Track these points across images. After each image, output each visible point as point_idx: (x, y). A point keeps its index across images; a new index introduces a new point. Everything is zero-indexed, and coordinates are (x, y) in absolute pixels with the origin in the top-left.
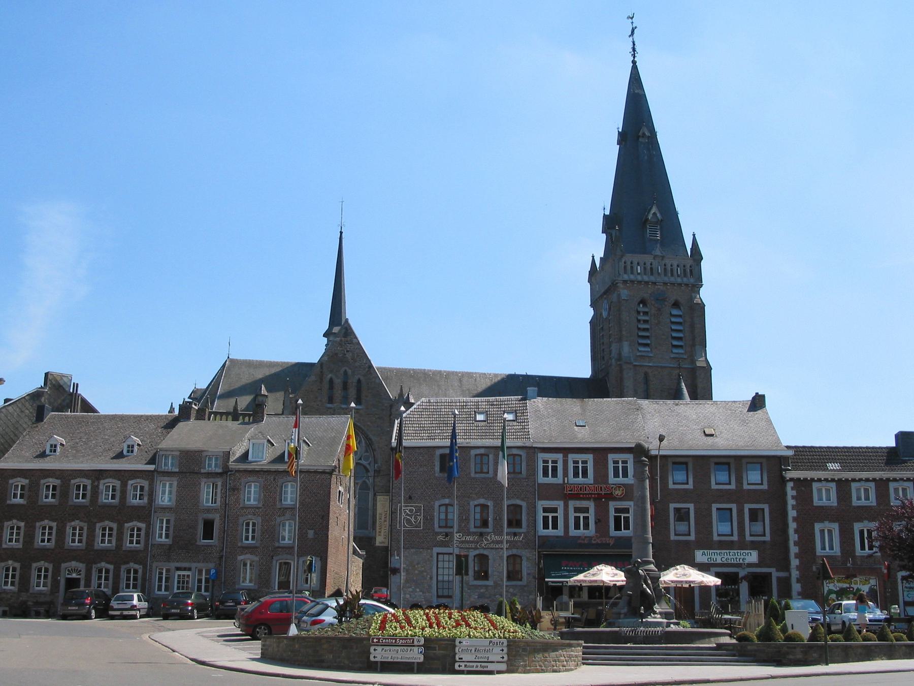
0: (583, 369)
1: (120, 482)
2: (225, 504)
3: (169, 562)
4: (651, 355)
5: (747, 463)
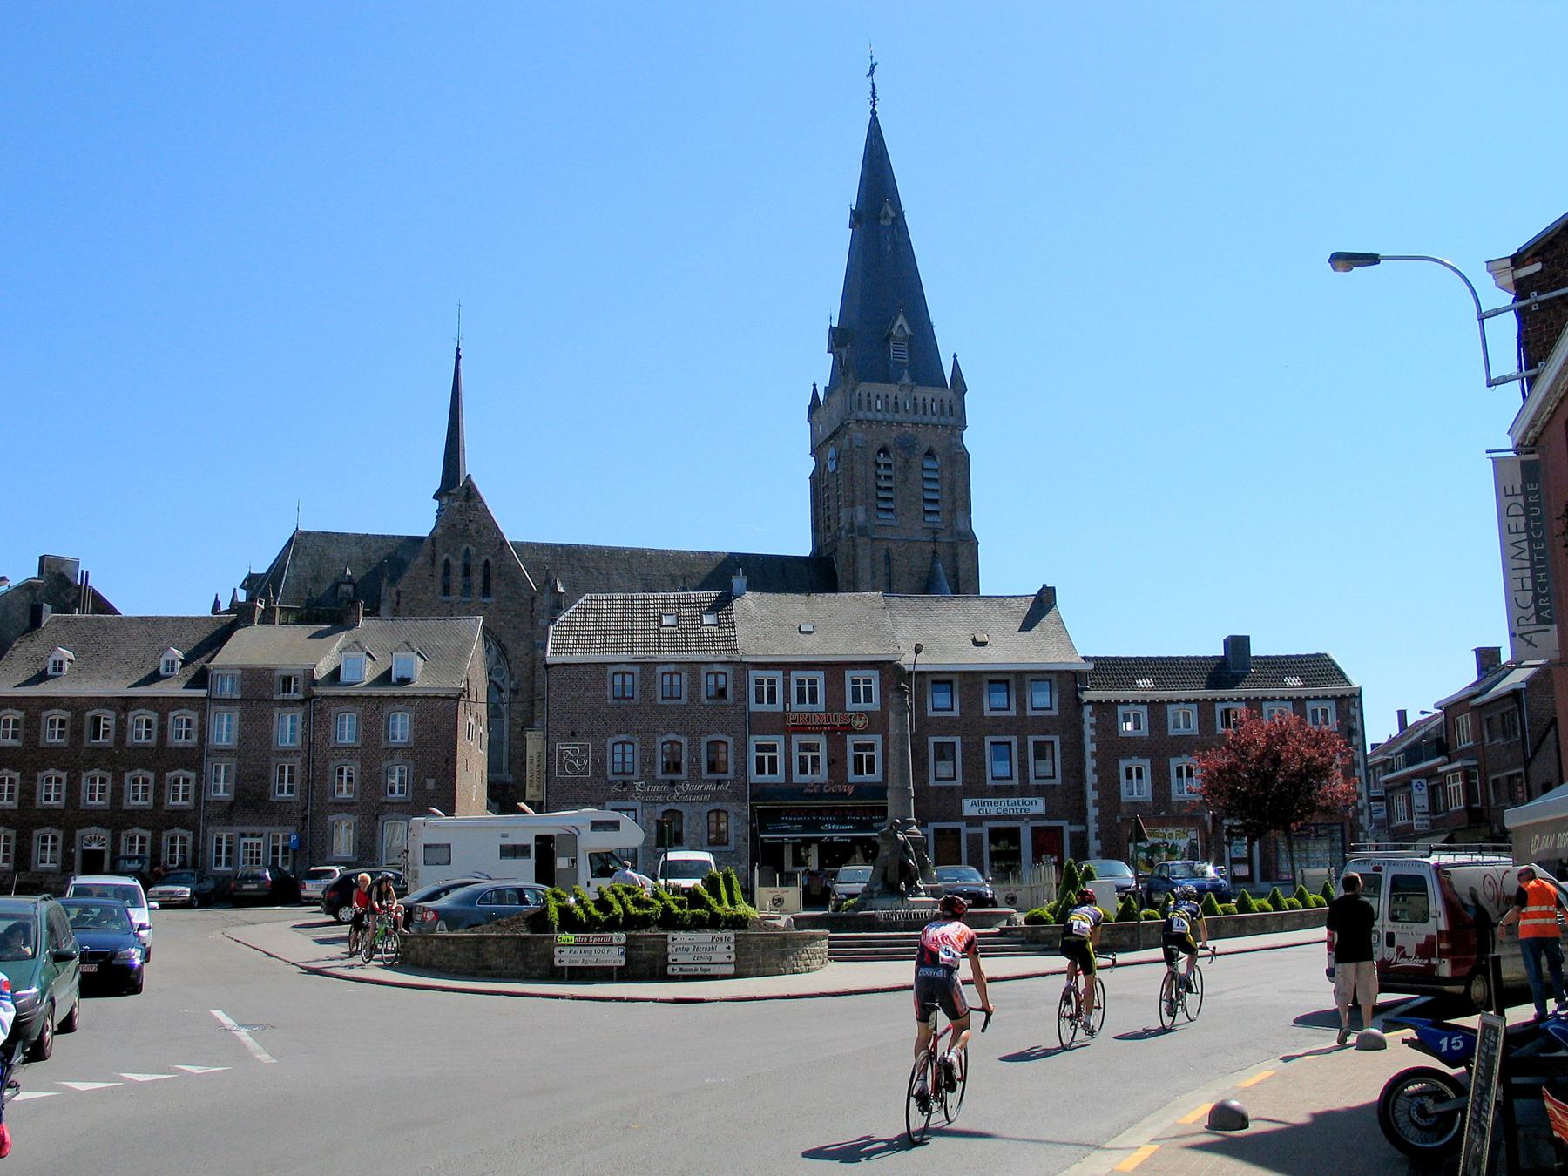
0: (799, 543)
1: (157, 714)
2: (310, 745)
4: (896, 524)
5: (1032, 680)
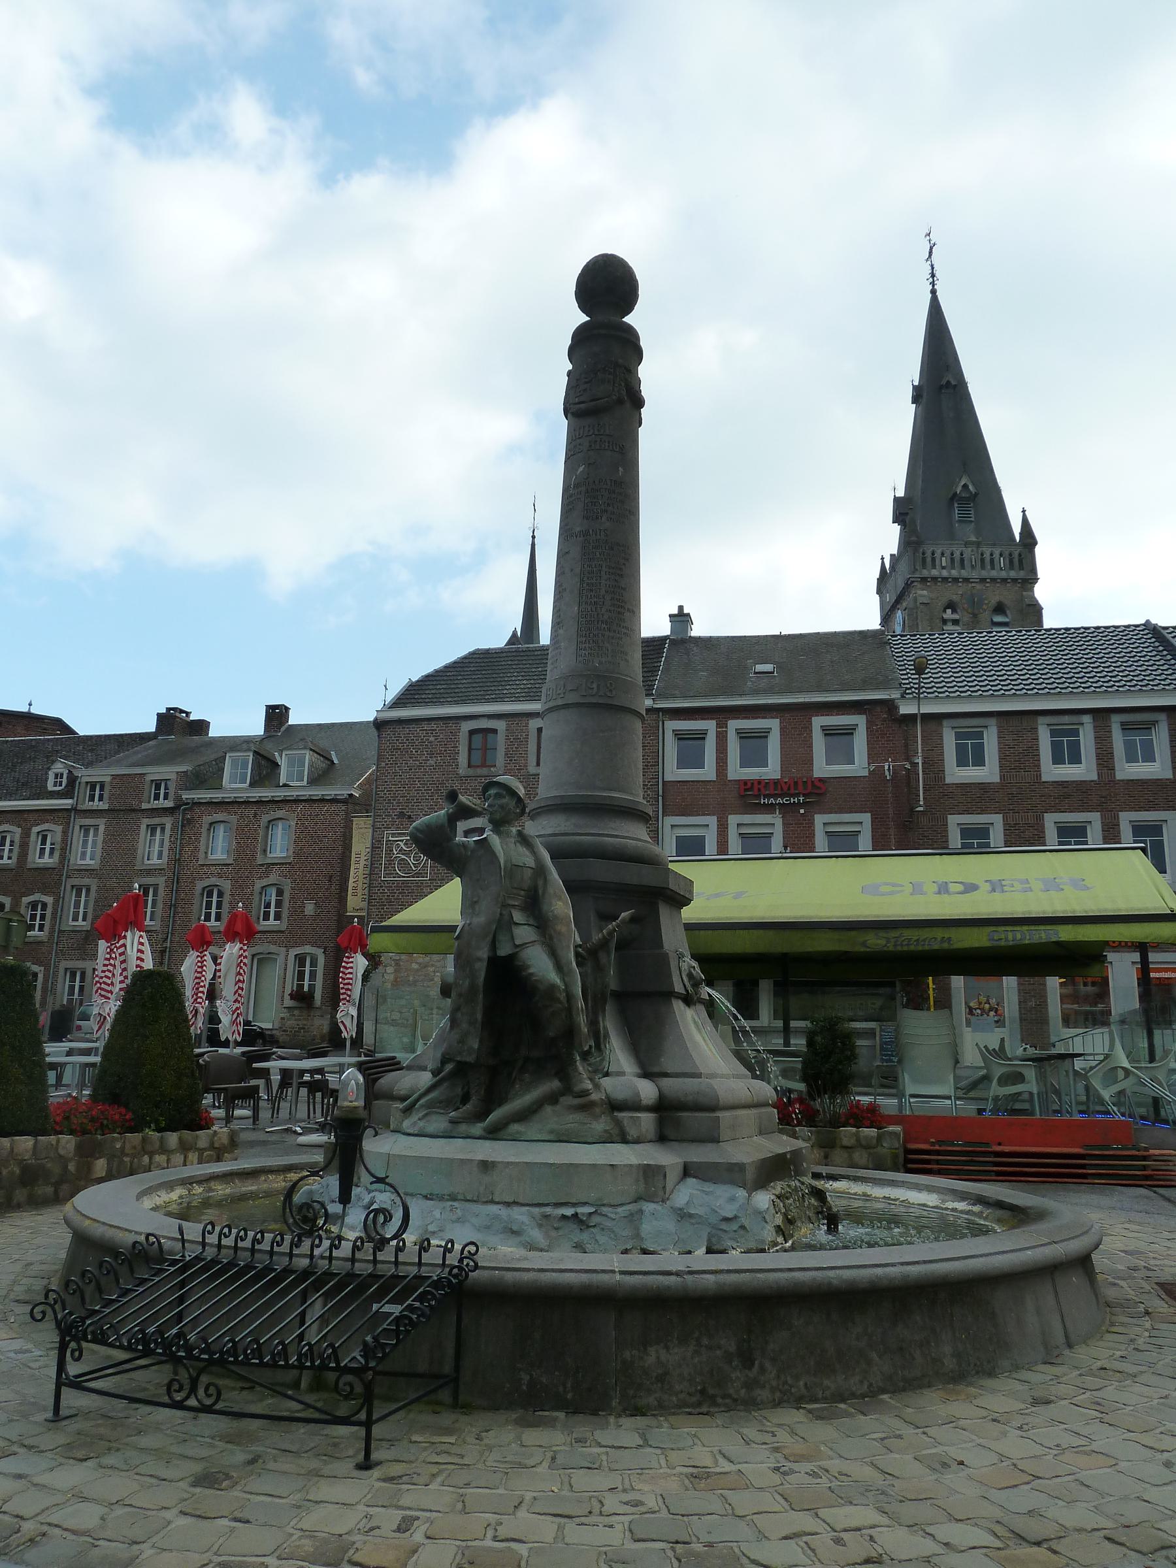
2: (176, 861)
3: (84, 959)
